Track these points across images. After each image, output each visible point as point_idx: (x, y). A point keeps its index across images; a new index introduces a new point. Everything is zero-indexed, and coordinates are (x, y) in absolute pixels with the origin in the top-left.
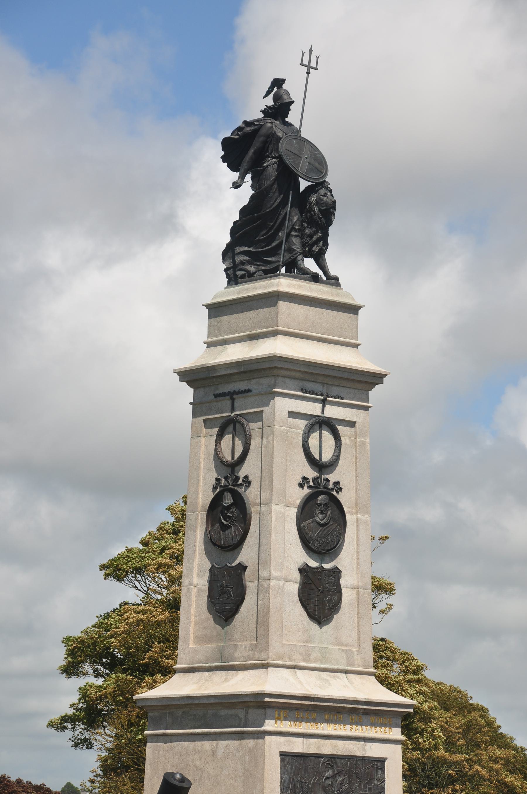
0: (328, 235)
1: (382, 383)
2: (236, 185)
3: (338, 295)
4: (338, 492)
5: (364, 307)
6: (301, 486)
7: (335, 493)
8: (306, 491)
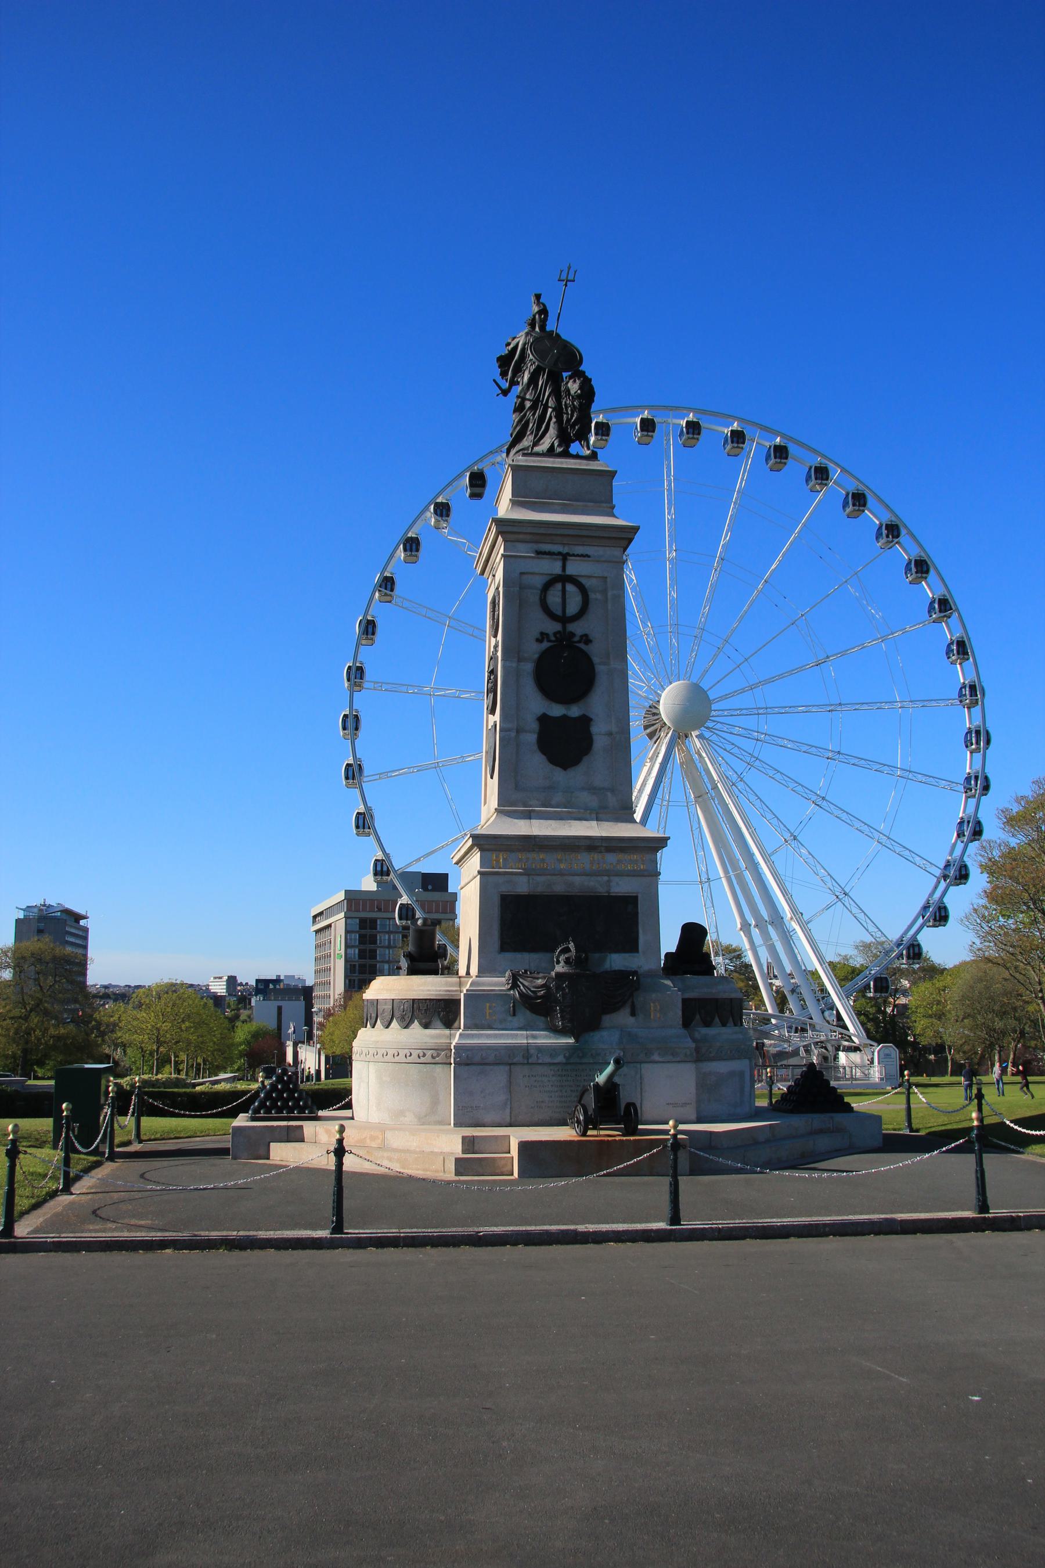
6: (539, 641)
7: (582, 646)
8: (546, 645)
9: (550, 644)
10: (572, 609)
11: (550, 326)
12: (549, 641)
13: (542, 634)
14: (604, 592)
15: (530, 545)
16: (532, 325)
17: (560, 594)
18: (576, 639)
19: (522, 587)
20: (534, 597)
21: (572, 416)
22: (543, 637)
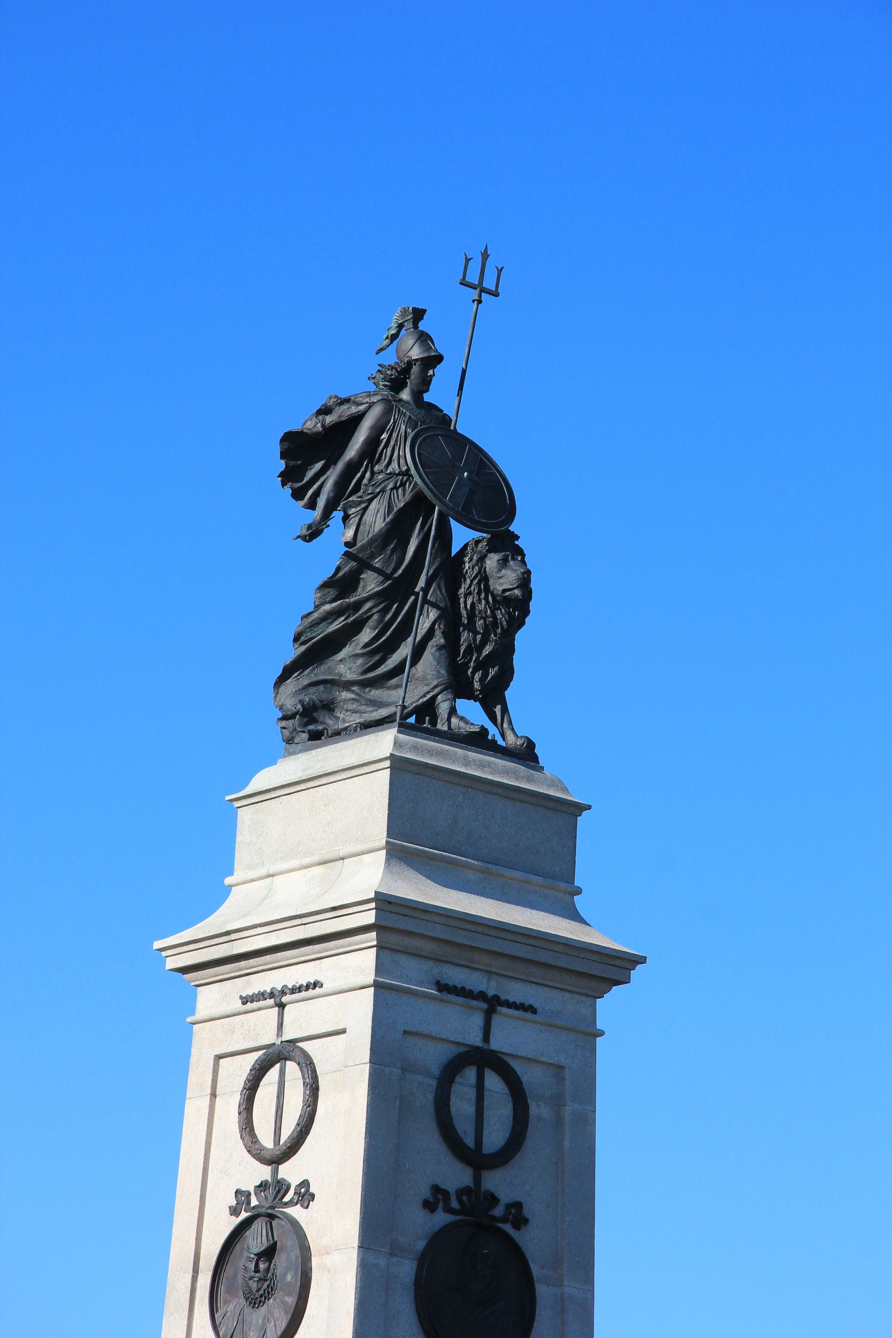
0: (512, 650)
1: (627, 981)
2: (313, 533)
3: (530, 780)
4: (517, 1227)
5: (589, 807)
6: (429, 1206)
7: (508, 1228)
8: (441, 1218)
9: (449, 1218)
10: (495, 1137)
11: (439, 394)
12: (449, 1210)
13: (436, 1190)
14: (557, 1101)
15: (428, 965)
16: (397, 385)
17: (472, 1094)
18: (498, 1211)
19: (407, 1068)
20: (425, 1099)
21: (484, 643)
22: (436, 1199)
